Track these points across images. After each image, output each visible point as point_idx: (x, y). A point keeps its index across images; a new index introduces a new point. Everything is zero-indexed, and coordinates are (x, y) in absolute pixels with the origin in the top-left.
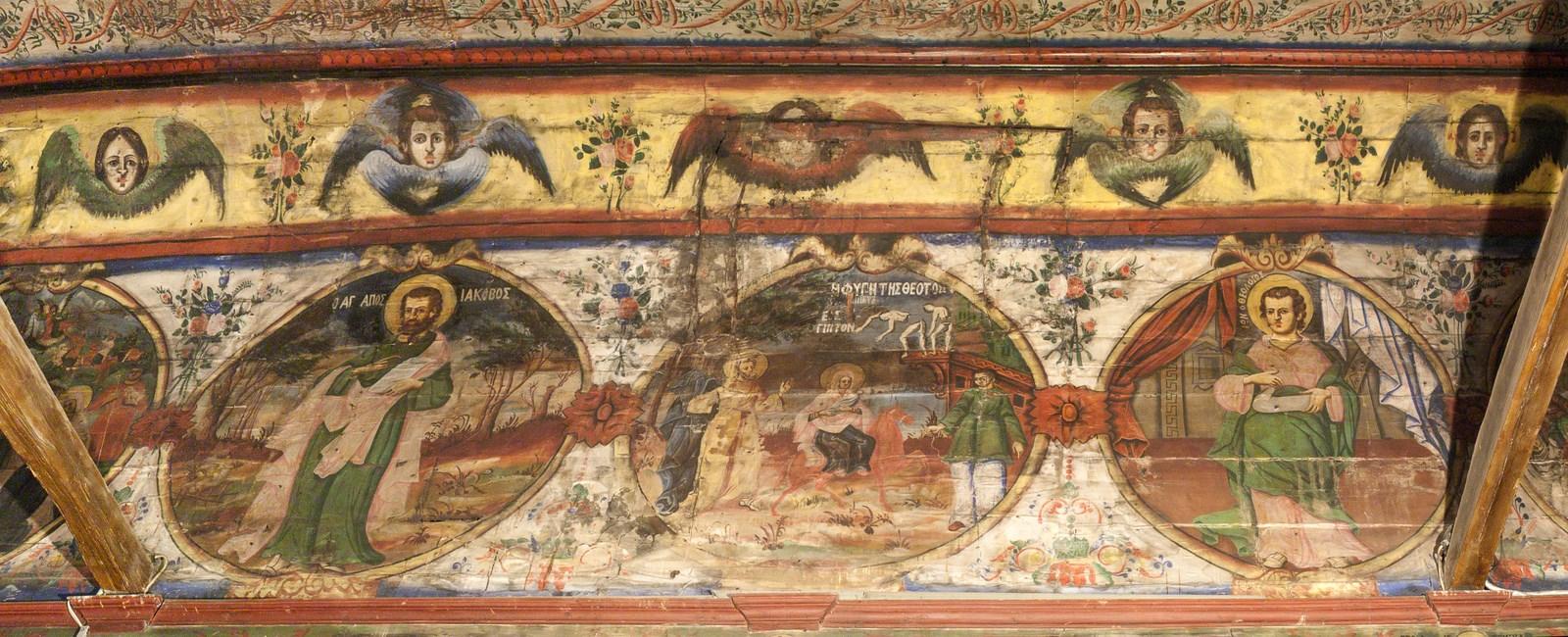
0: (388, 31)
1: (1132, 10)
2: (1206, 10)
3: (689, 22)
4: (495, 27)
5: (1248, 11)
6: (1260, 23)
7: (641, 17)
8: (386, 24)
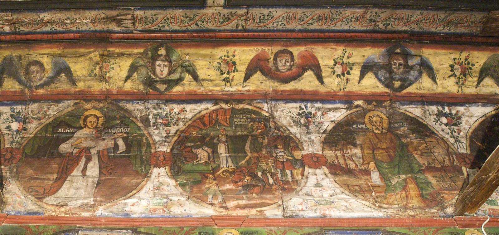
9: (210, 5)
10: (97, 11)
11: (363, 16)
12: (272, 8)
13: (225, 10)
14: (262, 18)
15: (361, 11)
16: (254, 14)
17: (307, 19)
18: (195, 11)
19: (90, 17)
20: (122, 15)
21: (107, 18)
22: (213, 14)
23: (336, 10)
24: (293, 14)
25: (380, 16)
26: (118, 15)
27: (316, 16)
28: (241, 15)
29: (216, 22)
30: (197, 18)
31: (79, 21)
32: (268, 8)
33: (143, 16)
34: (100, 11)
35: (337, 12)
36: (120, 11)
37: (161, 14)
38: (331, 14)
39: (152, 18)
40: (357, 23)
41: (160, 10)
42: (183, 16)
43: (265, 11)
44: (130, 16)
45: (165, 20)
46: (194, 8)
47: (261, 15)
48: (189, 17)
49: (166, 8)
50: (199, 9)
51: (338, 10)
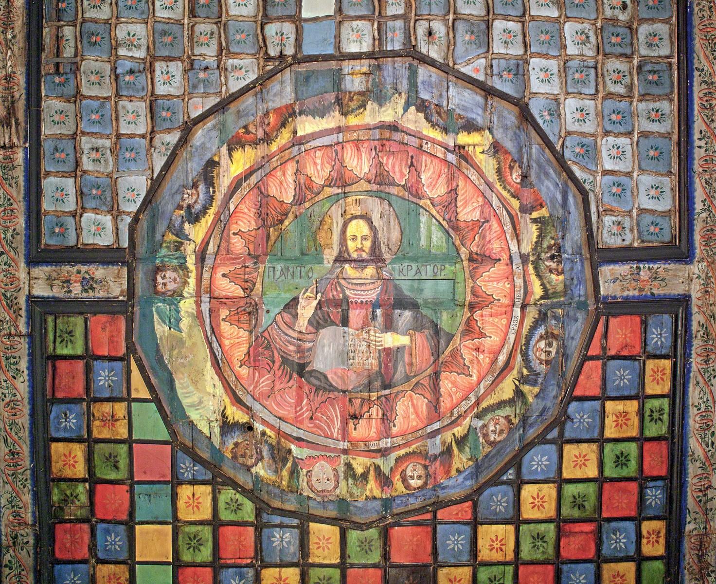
0: (711, 569)
1: (706, 160)
2: (705, 117)
3: (711, 405)
4: (711, 509)
5: (705, 91)
6: (712, 83)
7: (708, 430)
8: (707, 569)
9: (32, 273)
10: (25, 85)
11: (23, 523)
12: (29, 375)
13: (24, 298)
14: (12, 360)
15: (29, 518)
16: (19, 346)
17: (13, 434)
18: (22, 249)
19: (14, 73)
20: (17, 127)
21: (13, 102)
22: (18, 279)
23: (29, 477)
24: (20, 410)
25: (22, 550)
26: (17, 124)
27: (19, 449)
28: (17, 326)
29: (6, 285)
30: (12, 253)
31: (9, 54)
32: (28, 368)
33: (15, 163)
34: (24, 91)
35: (26, 480)
36: (23, 124)
37: (19, 192)
38: (22, 470)
39: (13, 178)
40: (11, 518)
41: (25, 190)
42: (14, 230)
43: (24, 365)
44: (15, 140)
45: (9, 200)
46: (26, 246)
47: (17, 359)
48: (14, 241)
49: (27, 201)
50: (25, 255)
51: (29, 481)
